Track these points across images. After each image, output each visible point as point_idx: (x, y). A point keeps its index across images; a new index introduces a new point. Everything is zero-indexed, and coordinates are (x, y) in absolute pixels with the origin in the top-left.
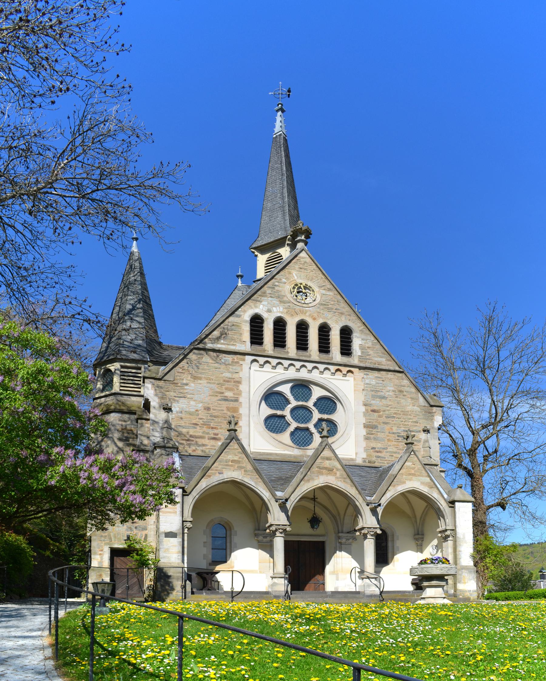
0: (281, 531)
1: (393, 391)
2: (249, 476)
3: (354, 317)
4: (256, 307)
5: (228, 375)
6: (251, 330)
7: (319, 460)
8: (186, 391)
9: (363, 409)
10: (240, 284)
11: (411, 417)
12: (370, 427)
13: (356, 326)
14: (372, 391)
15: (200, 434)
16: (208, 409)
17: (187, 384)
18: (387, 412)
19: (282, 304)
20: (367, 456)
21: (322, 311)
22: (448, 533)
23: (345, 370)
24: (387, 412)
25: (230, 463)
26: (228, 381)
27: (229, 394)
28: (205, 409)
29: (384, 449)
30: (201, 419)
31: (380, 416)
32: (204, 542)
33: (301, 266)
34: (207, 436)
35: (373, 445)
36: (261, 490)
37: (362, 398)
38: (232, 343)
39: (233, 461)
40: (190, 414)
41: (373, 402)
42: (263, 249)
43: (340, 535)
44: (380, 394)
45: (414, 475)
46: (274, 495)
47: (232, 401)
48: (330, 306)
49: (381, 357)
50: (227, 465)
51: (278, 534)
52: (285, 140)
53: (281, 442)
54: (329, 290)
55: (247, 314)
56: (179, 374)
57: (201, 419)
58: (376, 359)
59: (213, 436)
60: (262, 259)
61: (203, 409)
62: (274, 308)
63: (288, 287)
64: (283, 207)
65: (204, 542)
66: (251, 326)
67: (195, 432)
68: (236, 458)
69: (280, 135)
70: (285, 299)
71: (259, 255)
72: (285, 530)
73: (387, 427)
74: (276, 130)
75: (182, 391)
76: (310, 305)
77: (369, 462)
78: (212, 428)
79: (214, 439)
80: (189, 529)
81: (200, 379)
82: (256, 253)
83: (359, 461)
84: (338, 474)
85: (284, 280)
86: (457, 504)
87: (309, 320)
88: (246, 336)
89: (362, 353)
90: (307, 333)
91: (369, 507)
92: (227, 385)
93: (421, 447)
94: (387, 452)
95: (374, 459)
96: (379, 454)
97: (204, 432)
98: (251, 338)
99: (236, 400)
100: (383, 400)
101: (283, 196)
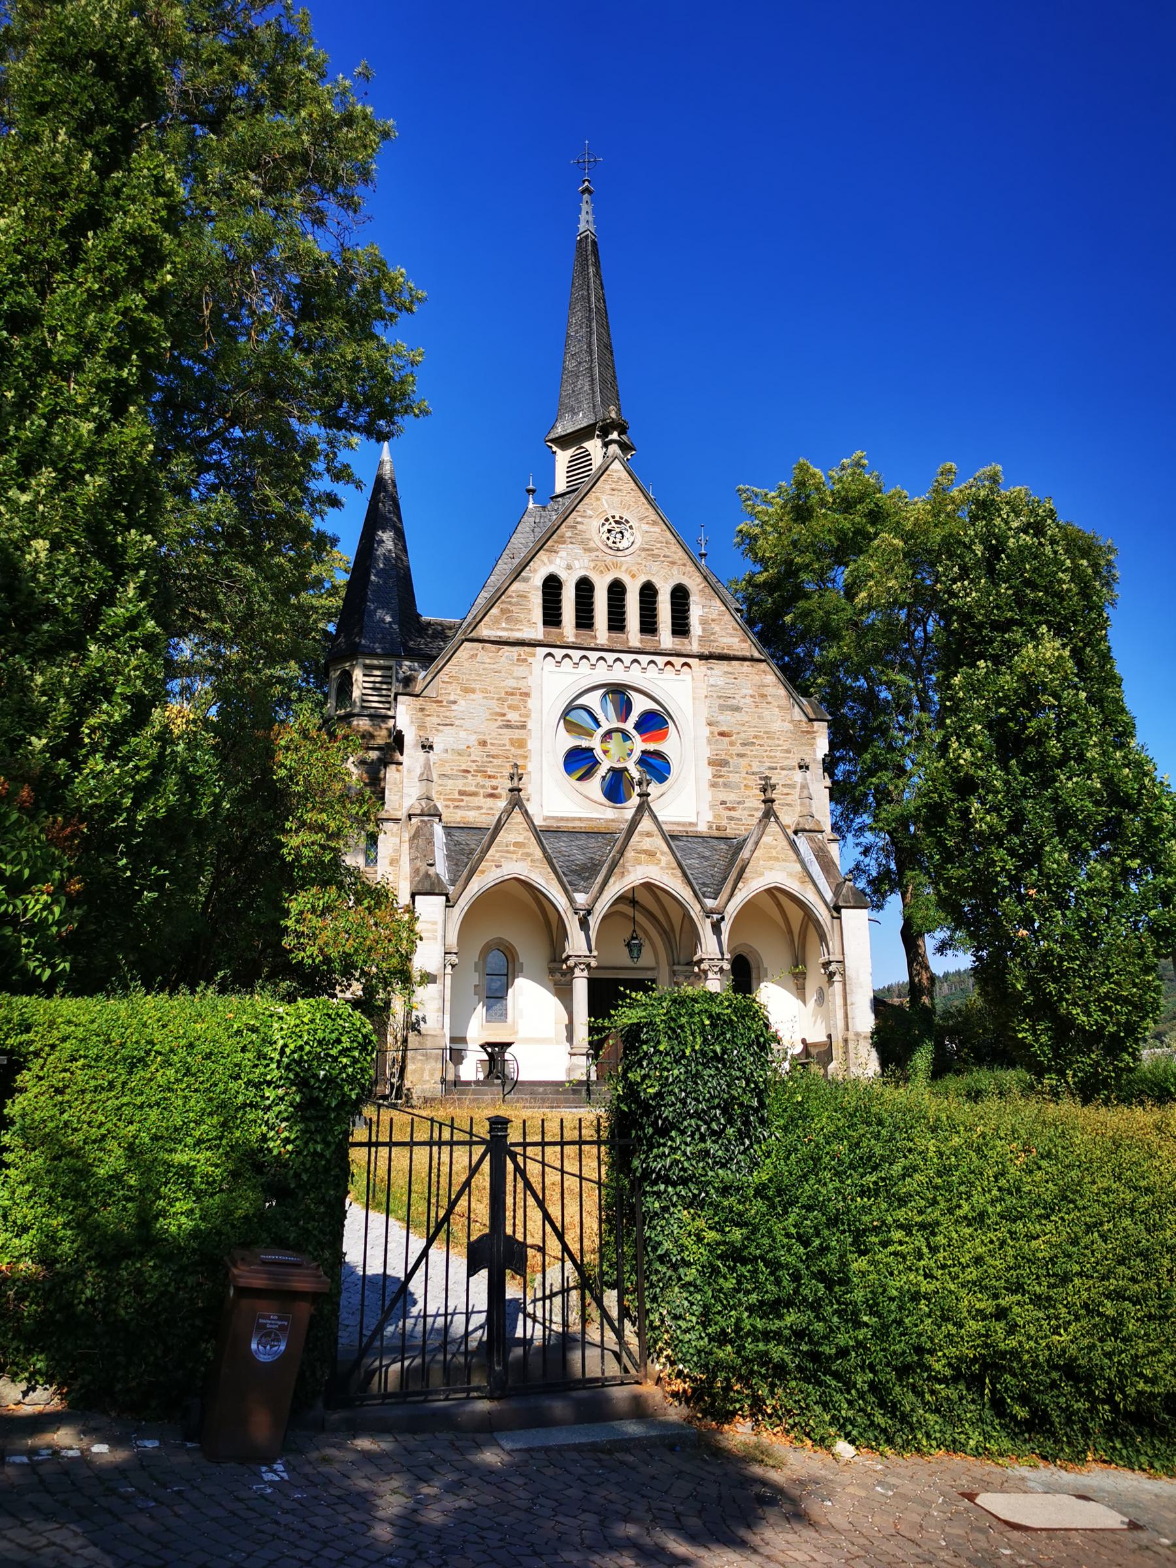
0: (582, 967)
1: (752, 696)
2: (537, 870)
3: (691, 568)
4: (551, 562)
5: (512, 683)
6: (545, 601)
7: (635, 838)
8: (453, 714)
9: (706, 731)
10: (531, 506)
11: (781, 742)
12: (718, 763)
13: (694, 583)
14: (720, 697)
15: (473, 789)
16: (484, 743)
17: (455, 702)
18: (742, 735)
19: (588, 554)
20: (715, 817)
21: (644, 563)
22: (833, 968)
23: (677, 662)
24: (742, 735)
25: (512, 848)
26: (512, 694)
27: (513, 716)
28: (480, 744)
29: (739, 803)
30: (474, 761)
31: (732, 744)
32: (476, 986)
33: (613, 486)
34: (482, 791)
35: (723, 796)
36: (554, 893)
37: (704, 714)
38: (518, 627)
39: (516, 844)
40: (460, 755)
41: (721, 718)
42: (565, 442)
43: (676, 968)
44: (731, 702)
45: (777, 859)
46: (571, 901)
47: (517, 727)
48: (656, 552)
49: (732, 636)
50: (508, 852)
51: (577, 972)
52: (594, 243)
53: (587, 798)
54: (654, 523)
55: (537, 576)
56: (444, 685)
57: (474, 761)
58: (725, 640)
59: (490, 791)
60: (563, 458)
61: (476, 743)
62: (576, 562)
63: (596, 523)
64: (591, 368)
65: (476, 986)
66: (544, 593)
67: (465, 785)
68: (520, 839)
69: (587, 236)
70: (592, 545)
71: (559, 451)
72: (588, 966)
73: (743, 762)
74: (582, 227)
75: (448, 714)
76: (627, 552)
77: (718, 829)
78: (490, 777)
79: (492, 796)
80: (453, 966)
81: (473, 691)
82: (555, 449)
83: (702, 828)
84: (664, 859)
85: (589, 512)
86: (843, 910)
87: (626, 579)
88: (537, 614)
89: (704, 630)
90: (623, 600)
91: (708, 921)
92: (511, 700)
93: (797, 797)
94: (744, 809)
95: (724, 823)
96: (732, 813)
97: (477, 785)
98: (545, 615)
99: (523, 727)
100: (736, 714)
101: (591, 350)
